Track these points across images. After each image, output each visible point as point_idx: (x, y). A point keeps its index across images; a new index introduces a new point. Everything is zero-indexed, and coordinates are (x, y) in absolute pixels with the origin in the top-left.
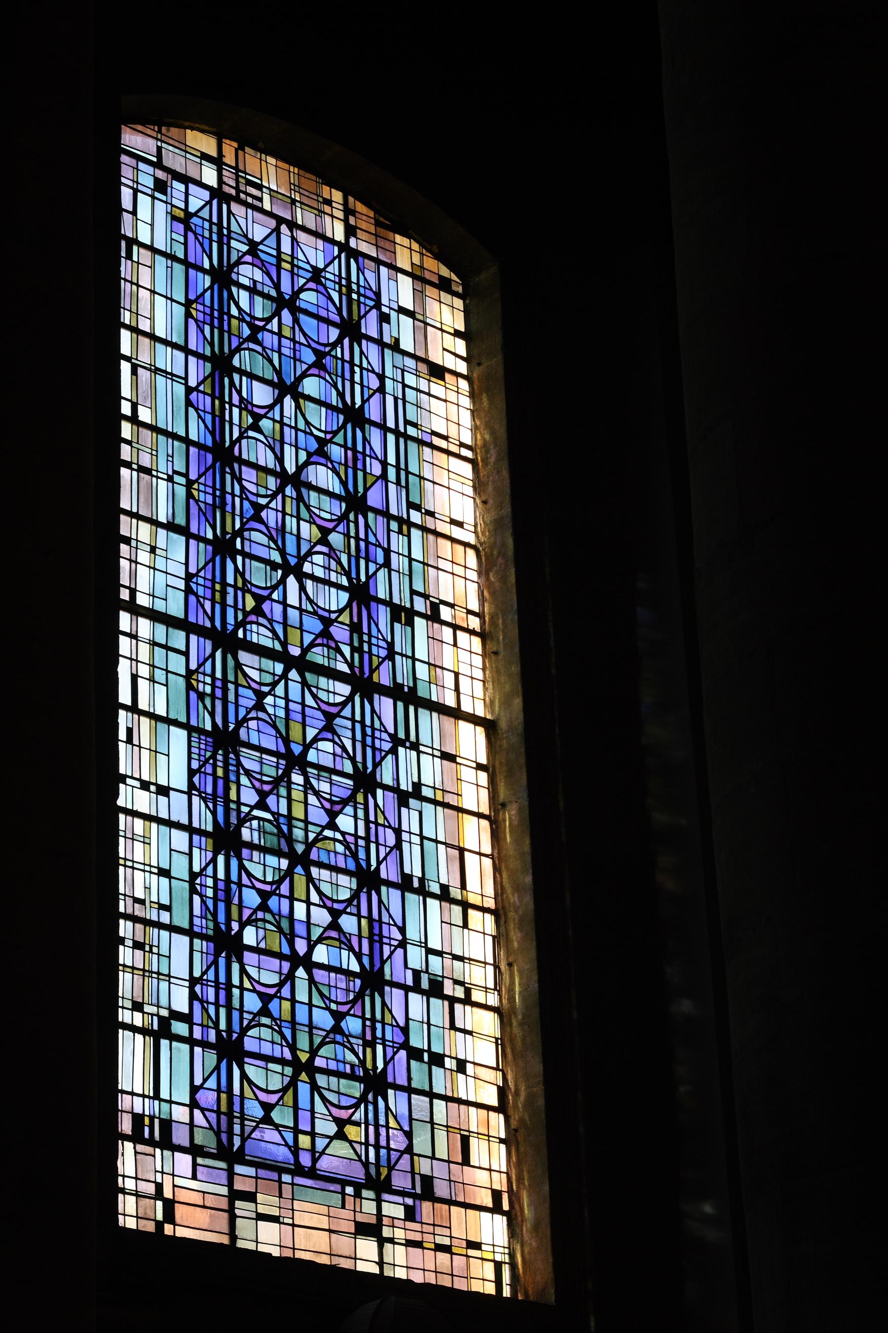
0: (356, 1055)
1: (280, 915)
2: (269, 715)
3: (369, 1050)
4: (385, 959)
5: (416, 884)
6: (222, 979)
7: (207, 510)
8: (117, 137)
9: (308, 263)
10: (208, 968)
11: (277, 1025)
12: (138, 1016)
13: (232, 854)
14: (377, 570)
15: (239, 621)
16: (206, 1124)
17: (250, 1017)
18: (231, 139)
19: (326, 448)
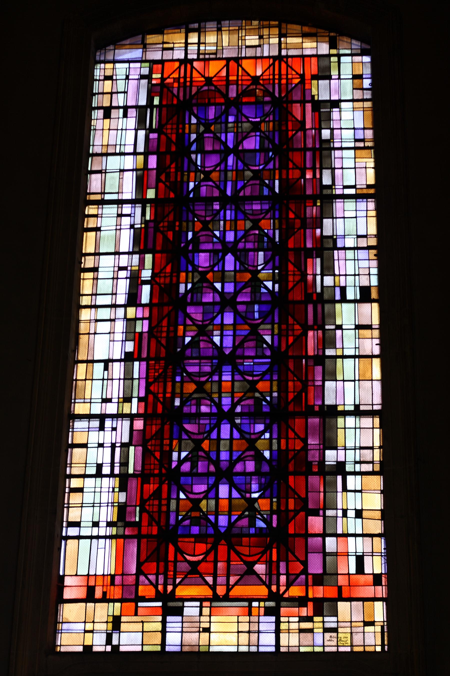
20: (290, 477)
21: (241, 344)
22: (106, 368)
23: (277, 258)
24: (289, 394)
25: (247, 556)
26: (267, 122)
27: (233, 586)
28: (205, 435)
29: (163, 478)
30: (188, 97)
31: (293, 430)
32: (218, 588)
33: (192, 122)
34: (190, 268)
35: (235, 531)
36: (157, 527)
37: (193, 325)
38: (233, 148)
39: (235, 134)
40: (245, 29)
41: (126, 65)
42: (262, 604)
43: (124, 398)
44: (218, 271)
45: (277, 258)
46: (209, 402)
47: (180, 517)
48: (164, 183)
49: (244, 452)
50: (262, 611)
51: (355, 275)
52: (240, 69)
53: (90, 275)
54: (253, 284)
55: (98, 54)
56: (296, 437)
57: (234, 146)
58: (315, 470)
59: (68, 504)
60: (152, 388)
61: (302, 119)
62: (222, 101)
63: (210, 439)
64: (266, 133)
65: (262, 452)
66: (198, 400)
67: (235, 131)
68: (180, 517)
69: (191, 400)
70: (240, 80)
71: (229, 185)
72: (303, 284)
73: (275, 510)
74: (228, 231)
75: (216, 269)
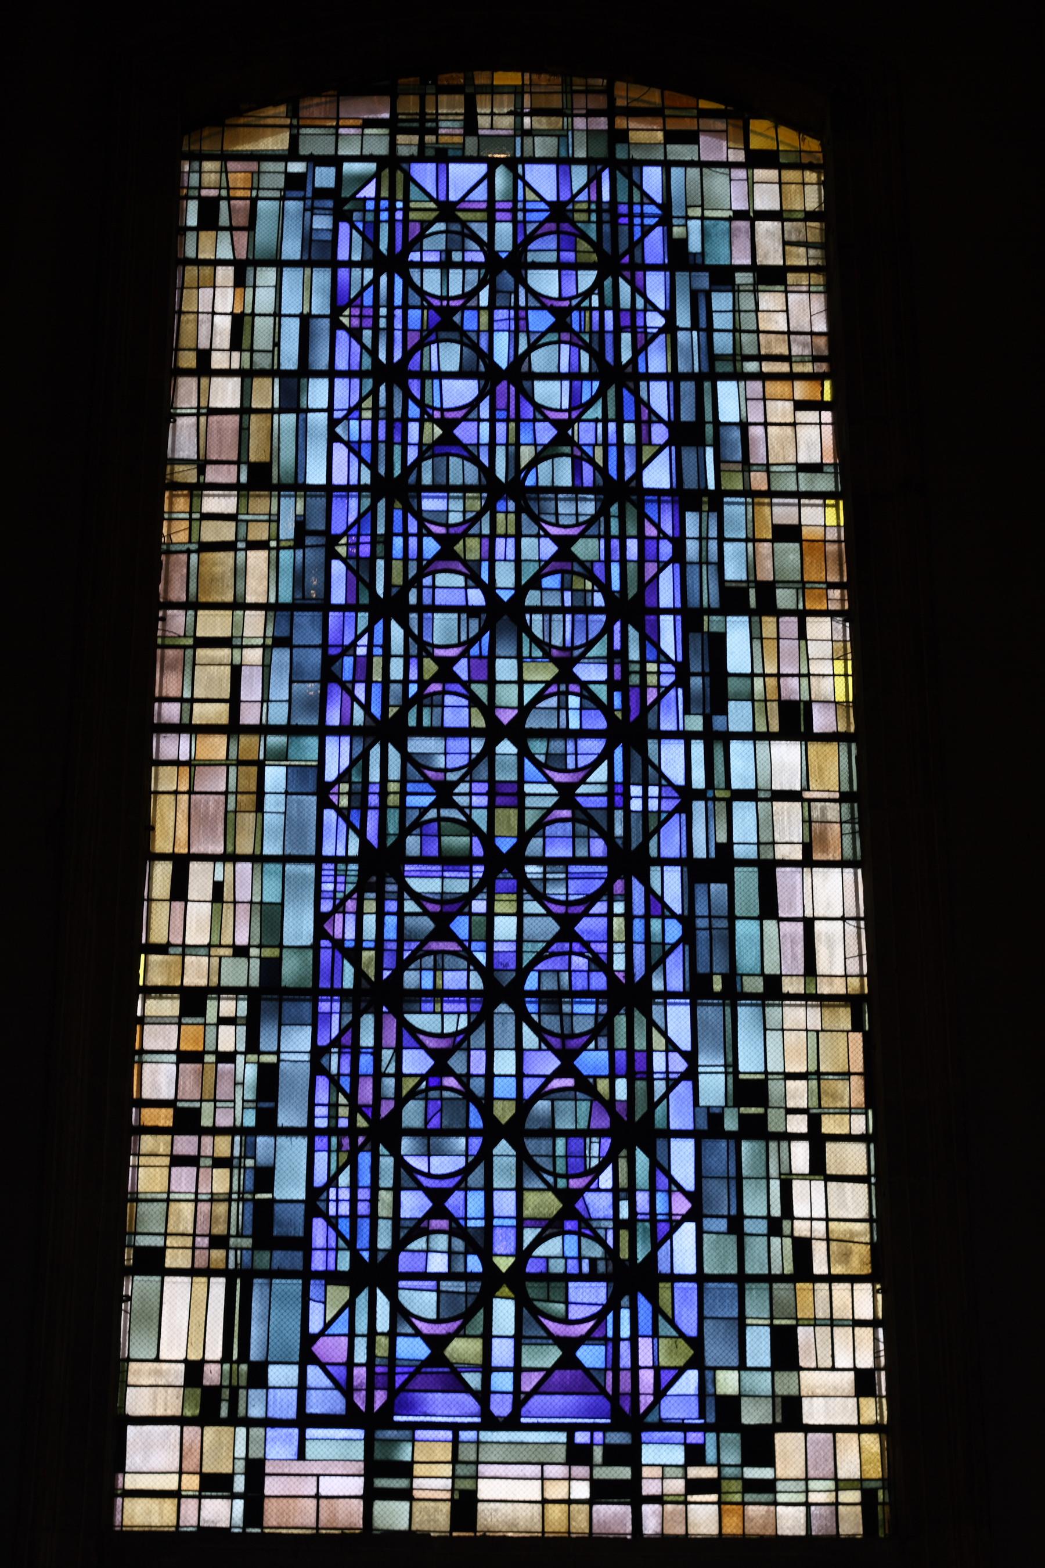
0: (602, 1242)
1: (469, 1075)
2: (461, 809)
3: (624, 1234)
4: (656, 1099)
5: (717, 985)
6: (397, 450)
7: (334, 825)
8: (177, 174)
9: (542, 199)
10: (340, 1170)
11: (457, 1229)
12: (218, 1255)
13: (385, 1009)
14: (660, 570)
15: (410, 696)
16: (327, 1383)
17: (414, 945)
18: (165, 474)
19: (570, 432)
20: (650, 741)
21: (535, 583)
22: (240, 282)
23: (618, 753)
24: (649, 690)
25: (556, 410)
26: (585, 309)
27: (529, 1395)
28: (458, 1039)
29: (361, 1140)
30: (397, 471)
31: (664, 1033)
32: (495, 1399)
33: (406, 910)
34: (413, 526)
35: (532, 1267)
36: (348, 1253)
37: (425, 781)
38: (507, 368)
39: (512, 335)
40: (531, 93)
41: (253, 166)
42: (598, 1436)
43: (274, 638)
44: (480, 657)
45: (618, 753)
46: (463, 964)
47: (406, 954)
48: (344, 560)
49: (550, 943)
50: (598, 1454)
51: (800, 675)
52: (520, 184)
53: (192, 317)
54: (563, 688)
55: (185, 142)
56: (662, 690)
57: (509, 365)
58: (717, 985)
59: (170, 512)
60: (339, 430)
61: (668, 308)
62: (480, 257)
63: (469, 658)
64: (583, 336)
65: (591, 1080)
66: (439, 957)
67: (513, 328)
68: (406, 954)
69: (421, 957)
70: (520, 210)
71: (500, 453)
72: (684, 816)
73: (624, 1221)
74: (500, 560)
75: (474, 651)
